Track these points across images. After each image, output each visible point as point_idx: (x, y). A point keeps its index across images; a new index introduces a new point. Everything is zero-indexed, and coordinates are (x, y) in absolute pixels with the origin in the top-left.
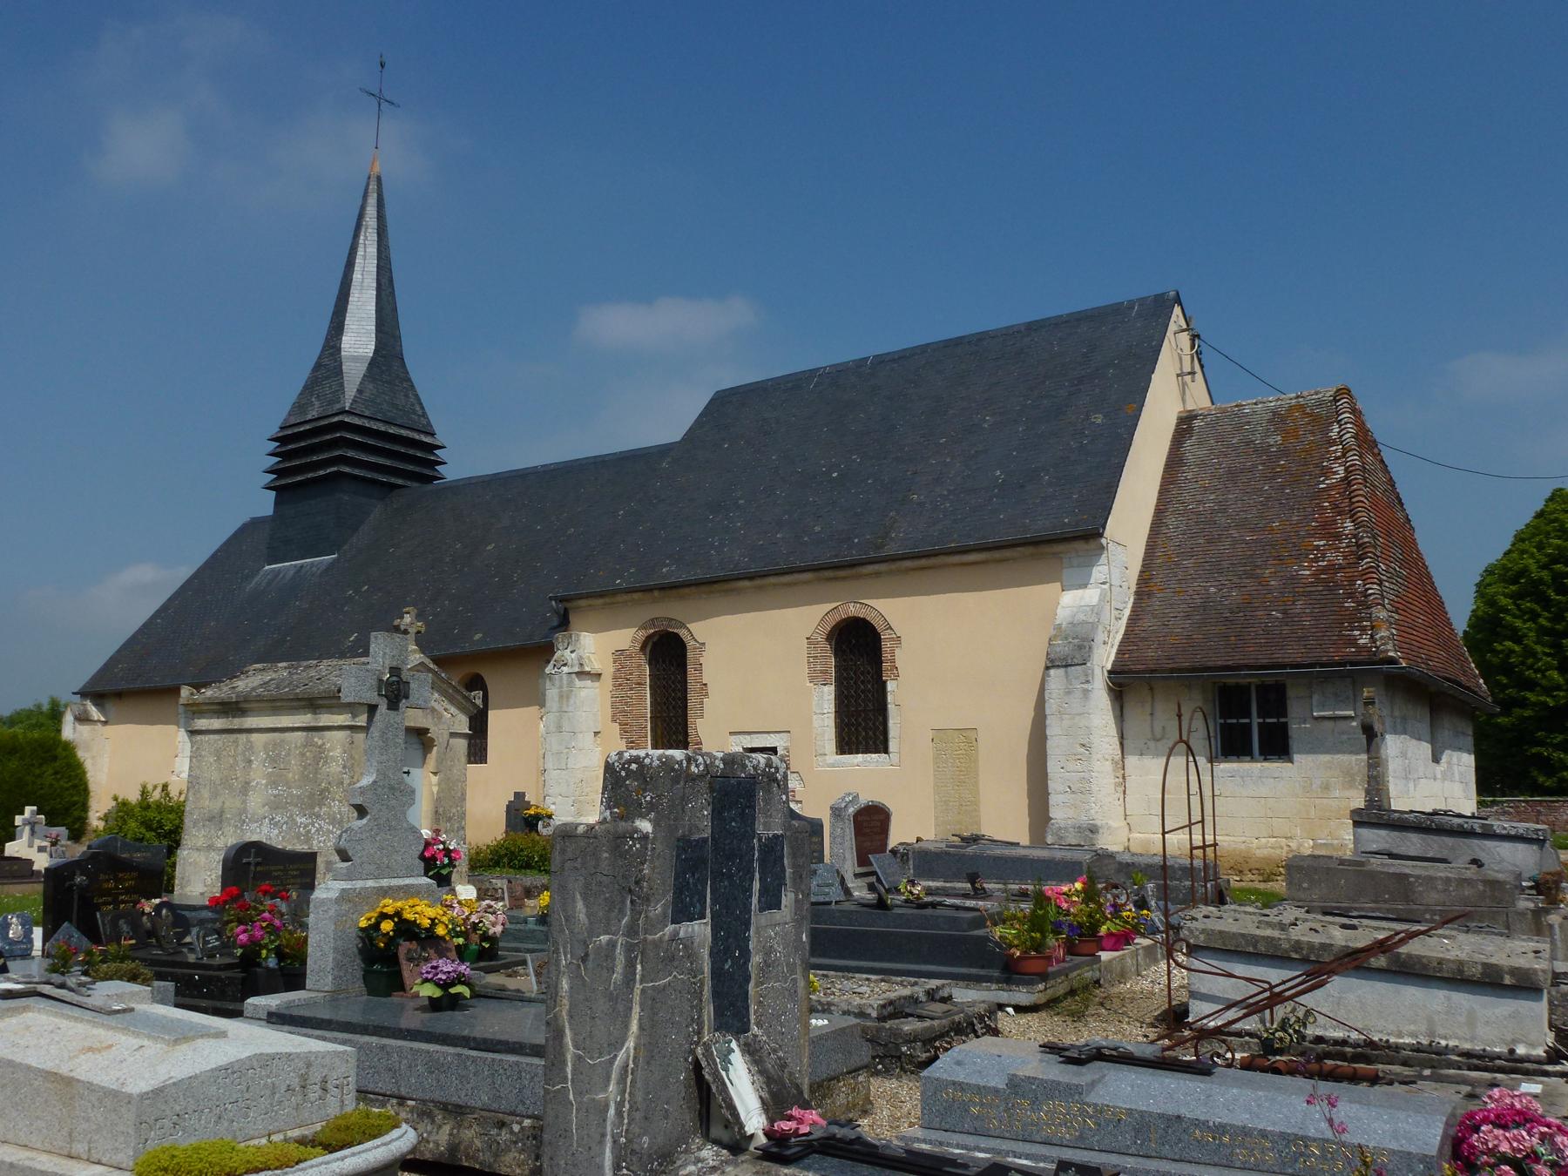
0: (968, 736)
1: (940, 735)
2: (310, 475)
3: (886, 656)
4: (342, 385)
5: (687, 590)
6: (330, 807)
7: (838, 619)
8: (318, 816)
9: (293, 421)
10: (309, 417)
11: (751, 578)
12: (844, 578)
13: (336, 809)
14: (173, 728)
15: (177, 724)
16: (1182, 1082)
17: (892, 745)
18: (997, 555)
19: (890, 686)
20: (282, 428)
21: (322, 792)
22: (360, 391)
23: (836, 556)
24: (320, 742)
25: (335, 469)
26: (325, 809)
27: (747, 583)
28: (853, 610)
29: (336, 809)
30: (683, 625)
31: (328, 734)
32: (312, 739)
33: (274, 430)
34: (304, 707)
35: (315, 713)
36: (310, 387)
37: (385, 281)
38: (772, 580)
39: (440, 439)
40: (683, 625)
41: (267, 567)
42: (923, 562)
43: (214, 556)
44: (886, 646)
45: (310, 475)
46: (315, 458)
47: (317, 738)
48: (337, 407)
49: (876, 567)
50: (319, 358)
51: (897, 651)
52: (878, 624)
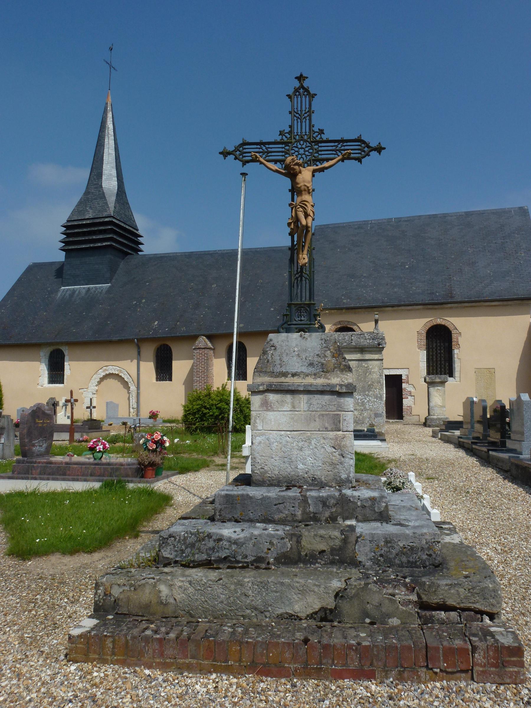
0: (491, 371)
1: (478, 371)
2: (92, 245)
3: (454, 339)
4: (106, 204)
5: (360, 310)
6: (374, 391)
7: (432, 325)
8: (368, 395)
9: (76, 218)
10: (87, 217)
11: (393, 306)
12: (436, 309)
13: (377, 393)
14: (38, 363)
15: (40, 361)
16: (106, 529)
17: (65, 382)
18: (505, 303)
19: (456, 351)
20: (68, 221)
21: (369, 386)
22: (115, 207)
23: (432, 300)
24: (366, 366)
25: (109, 243)
26: (371, 393)
27: (390, 309)
28: (439, 321)
29: (377, 393)
30: (355, 324)
31: (370, 362)
32: (362, 364)
33: (64, 221)
34: (356, 351)
35: (362, 354)
36: (83, 203)
37: (117, 155)
38: (403, 308)
39: (140, 232)
40: (355, 324)
41: (62, 288)
42: (474, 304)
43: (19, 280)
44: (454, 336)
45: (92, 245)
46: (94, 237)
47: (364, 364)
48: (105, 214)
49: (453, 305)
50: (87, 188)
51: (459, 338)
52: (451, 328)
